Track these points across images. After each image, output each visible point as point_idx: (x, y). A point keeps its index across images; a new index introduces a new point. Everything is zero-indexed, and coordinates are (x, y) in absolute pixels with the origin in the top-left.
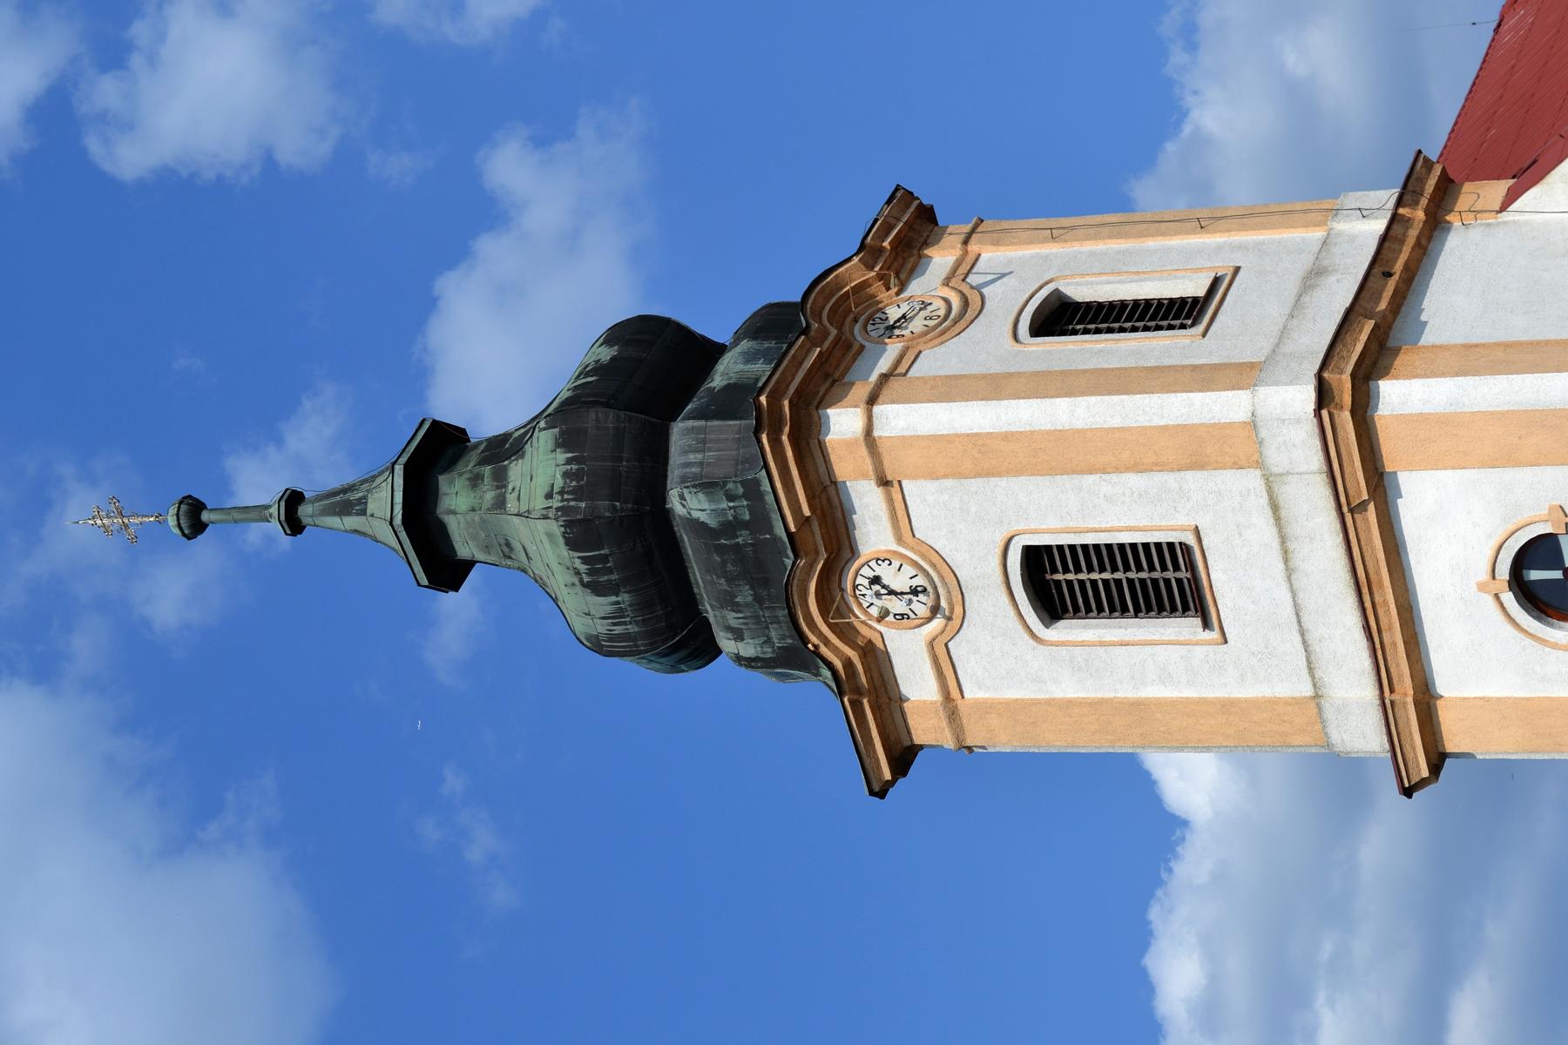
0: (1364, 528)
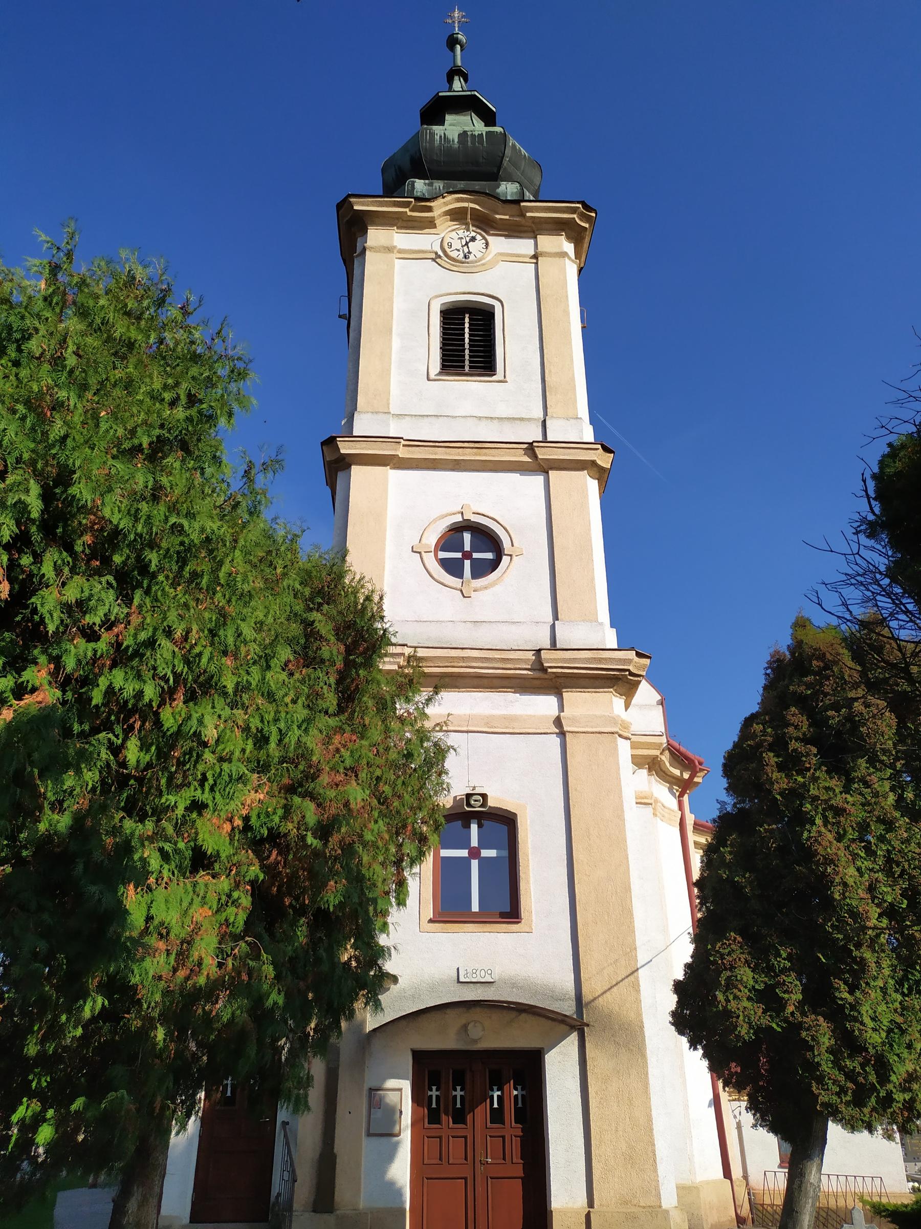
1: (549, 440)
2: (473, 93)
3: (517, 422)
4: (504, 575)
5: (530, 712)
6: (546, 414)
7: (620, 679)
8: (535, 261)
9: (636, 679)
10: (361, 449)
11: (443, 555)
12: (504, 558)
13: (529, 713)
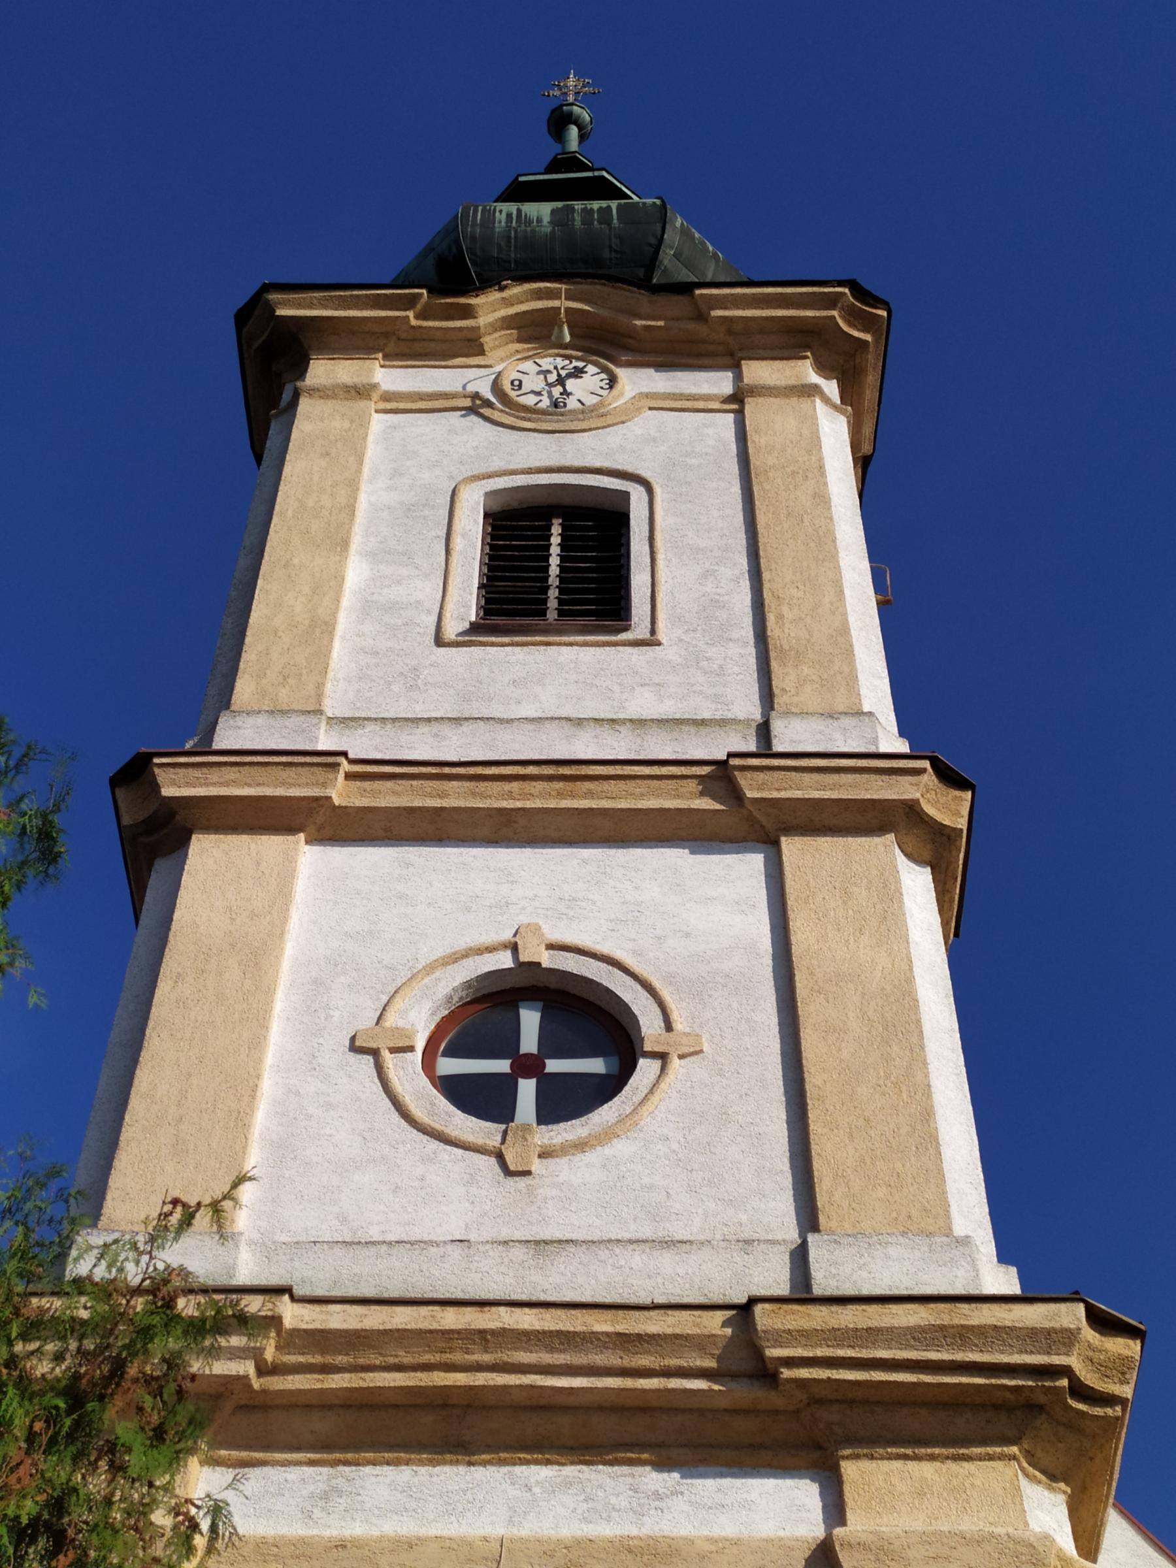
0: (682, 790)
1: (778, 747)
2: (596, 173)
3: (685, 728)
4: (644, 1111)
5: (726, 1527)
6: (768, 697)
7: (1041, 1408)
8: (735, 407)
9: (1098, 1411)
10: (221, 784)
11: (448, 1066)
12: (642, 1062)
13: (716, 1532)
